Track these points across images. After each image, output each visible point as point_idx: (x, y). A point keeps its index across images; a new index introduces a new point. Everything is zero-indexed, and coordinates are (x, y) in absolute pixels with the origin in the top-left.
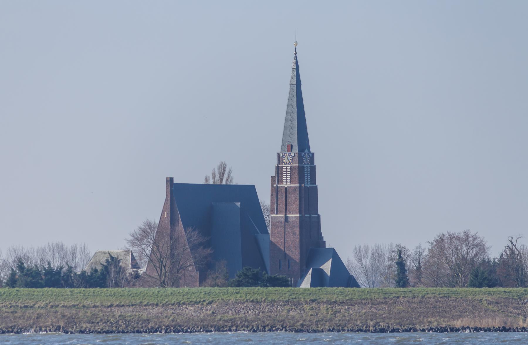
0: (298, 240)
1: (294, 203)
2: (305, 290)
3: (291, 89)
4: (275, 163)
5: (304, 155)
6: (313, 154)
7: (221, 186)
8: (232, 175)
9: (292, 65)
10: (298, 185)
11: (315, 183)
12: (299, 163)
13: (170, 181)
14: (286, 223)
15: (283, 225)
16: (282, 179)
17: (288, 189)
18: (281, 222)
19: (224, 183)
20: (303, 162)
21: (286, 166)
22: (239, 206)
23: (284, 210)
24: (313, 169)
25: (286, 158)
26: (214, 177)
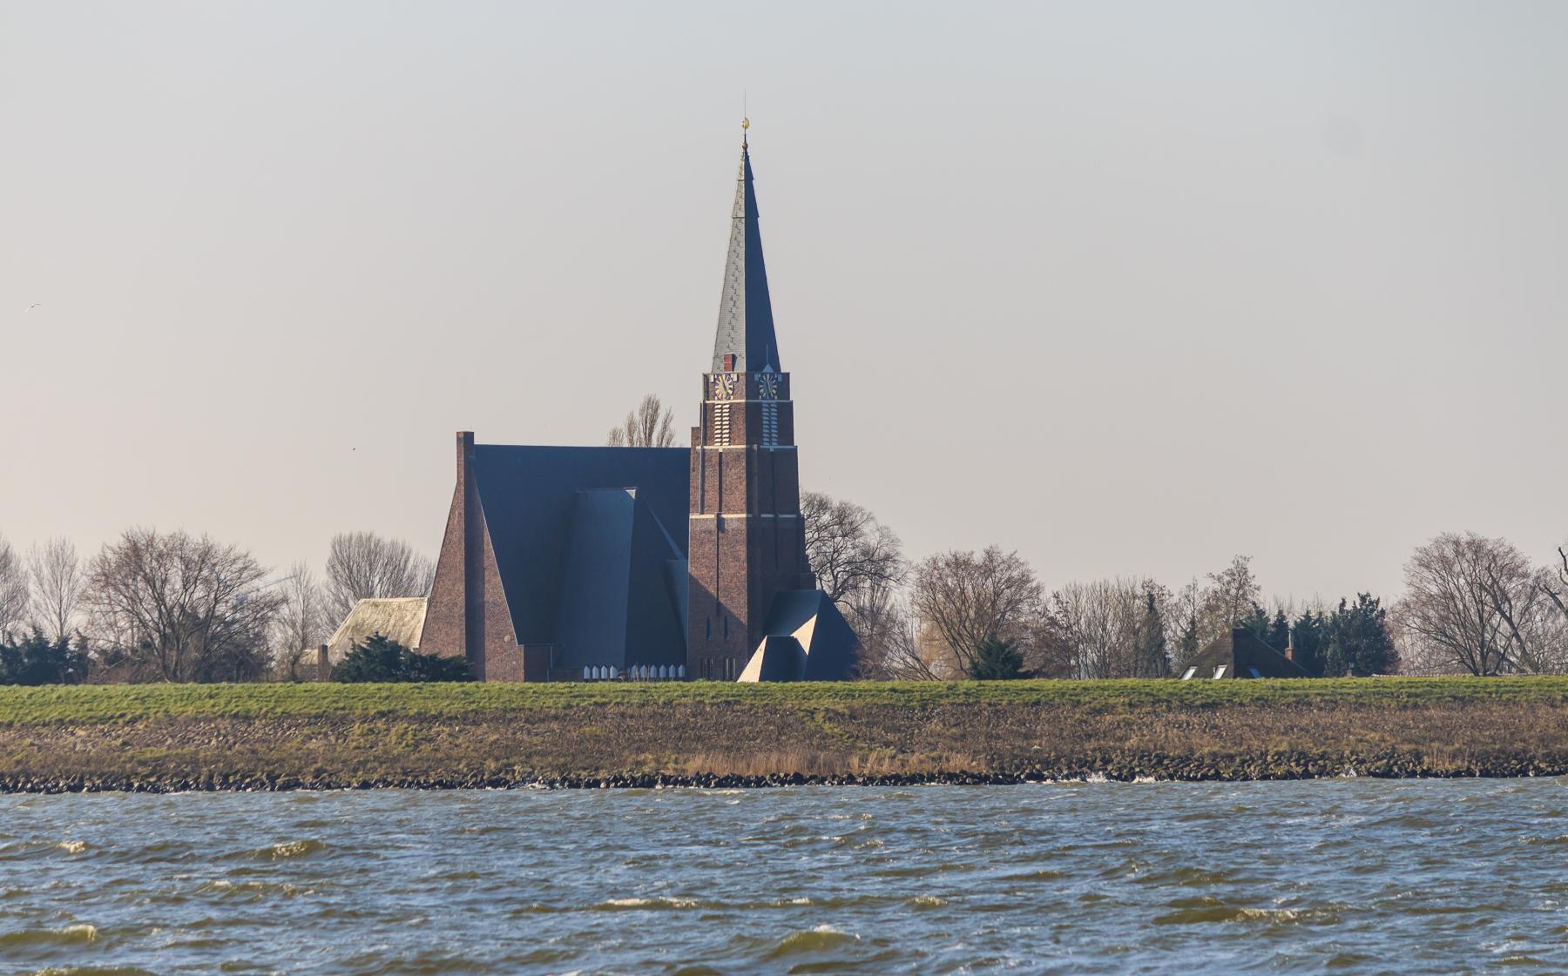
0: (744, 572)
1: (736, 488)
2: (746, 685)
3: (735, 226)
4: (699, 397)
5: (761, 378)
6: (787, 376)
7: (667, 449)
8: (672, 426)
9: (736, 172)
10: (744, 446)
11: (791, 442)
12: (748, 397)
13: (466, 439)
14: (720, 535)
15: (715, 537)
16: (713, 434)
17: (724, 456)
18: (710, 532)
19: (654, 444)
20: (759, 394)
21: (721, 402)
22: (634, 496)
23: (717, 505)
24: (786, 412)
25: (721, 384)
26: (631, 432)
